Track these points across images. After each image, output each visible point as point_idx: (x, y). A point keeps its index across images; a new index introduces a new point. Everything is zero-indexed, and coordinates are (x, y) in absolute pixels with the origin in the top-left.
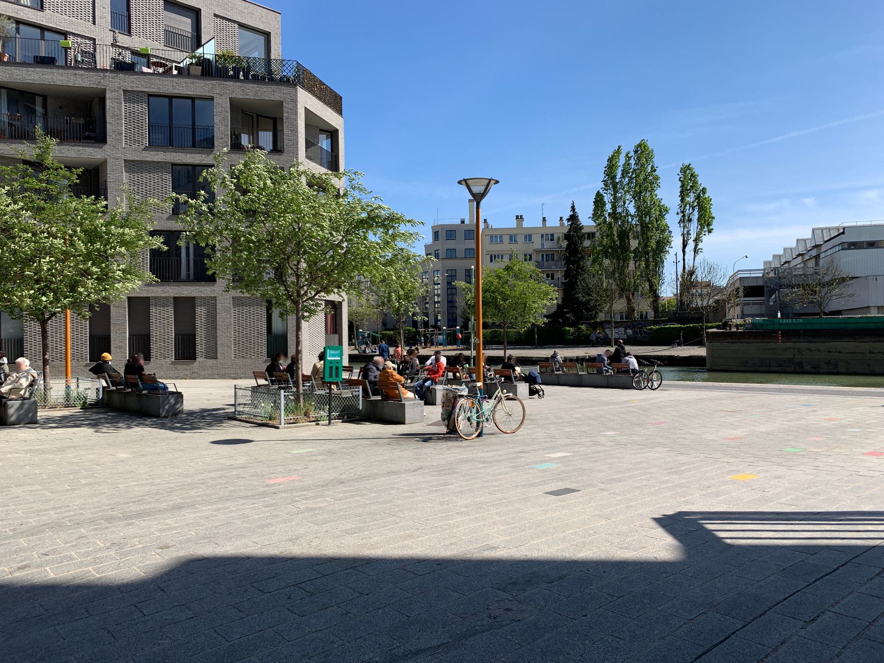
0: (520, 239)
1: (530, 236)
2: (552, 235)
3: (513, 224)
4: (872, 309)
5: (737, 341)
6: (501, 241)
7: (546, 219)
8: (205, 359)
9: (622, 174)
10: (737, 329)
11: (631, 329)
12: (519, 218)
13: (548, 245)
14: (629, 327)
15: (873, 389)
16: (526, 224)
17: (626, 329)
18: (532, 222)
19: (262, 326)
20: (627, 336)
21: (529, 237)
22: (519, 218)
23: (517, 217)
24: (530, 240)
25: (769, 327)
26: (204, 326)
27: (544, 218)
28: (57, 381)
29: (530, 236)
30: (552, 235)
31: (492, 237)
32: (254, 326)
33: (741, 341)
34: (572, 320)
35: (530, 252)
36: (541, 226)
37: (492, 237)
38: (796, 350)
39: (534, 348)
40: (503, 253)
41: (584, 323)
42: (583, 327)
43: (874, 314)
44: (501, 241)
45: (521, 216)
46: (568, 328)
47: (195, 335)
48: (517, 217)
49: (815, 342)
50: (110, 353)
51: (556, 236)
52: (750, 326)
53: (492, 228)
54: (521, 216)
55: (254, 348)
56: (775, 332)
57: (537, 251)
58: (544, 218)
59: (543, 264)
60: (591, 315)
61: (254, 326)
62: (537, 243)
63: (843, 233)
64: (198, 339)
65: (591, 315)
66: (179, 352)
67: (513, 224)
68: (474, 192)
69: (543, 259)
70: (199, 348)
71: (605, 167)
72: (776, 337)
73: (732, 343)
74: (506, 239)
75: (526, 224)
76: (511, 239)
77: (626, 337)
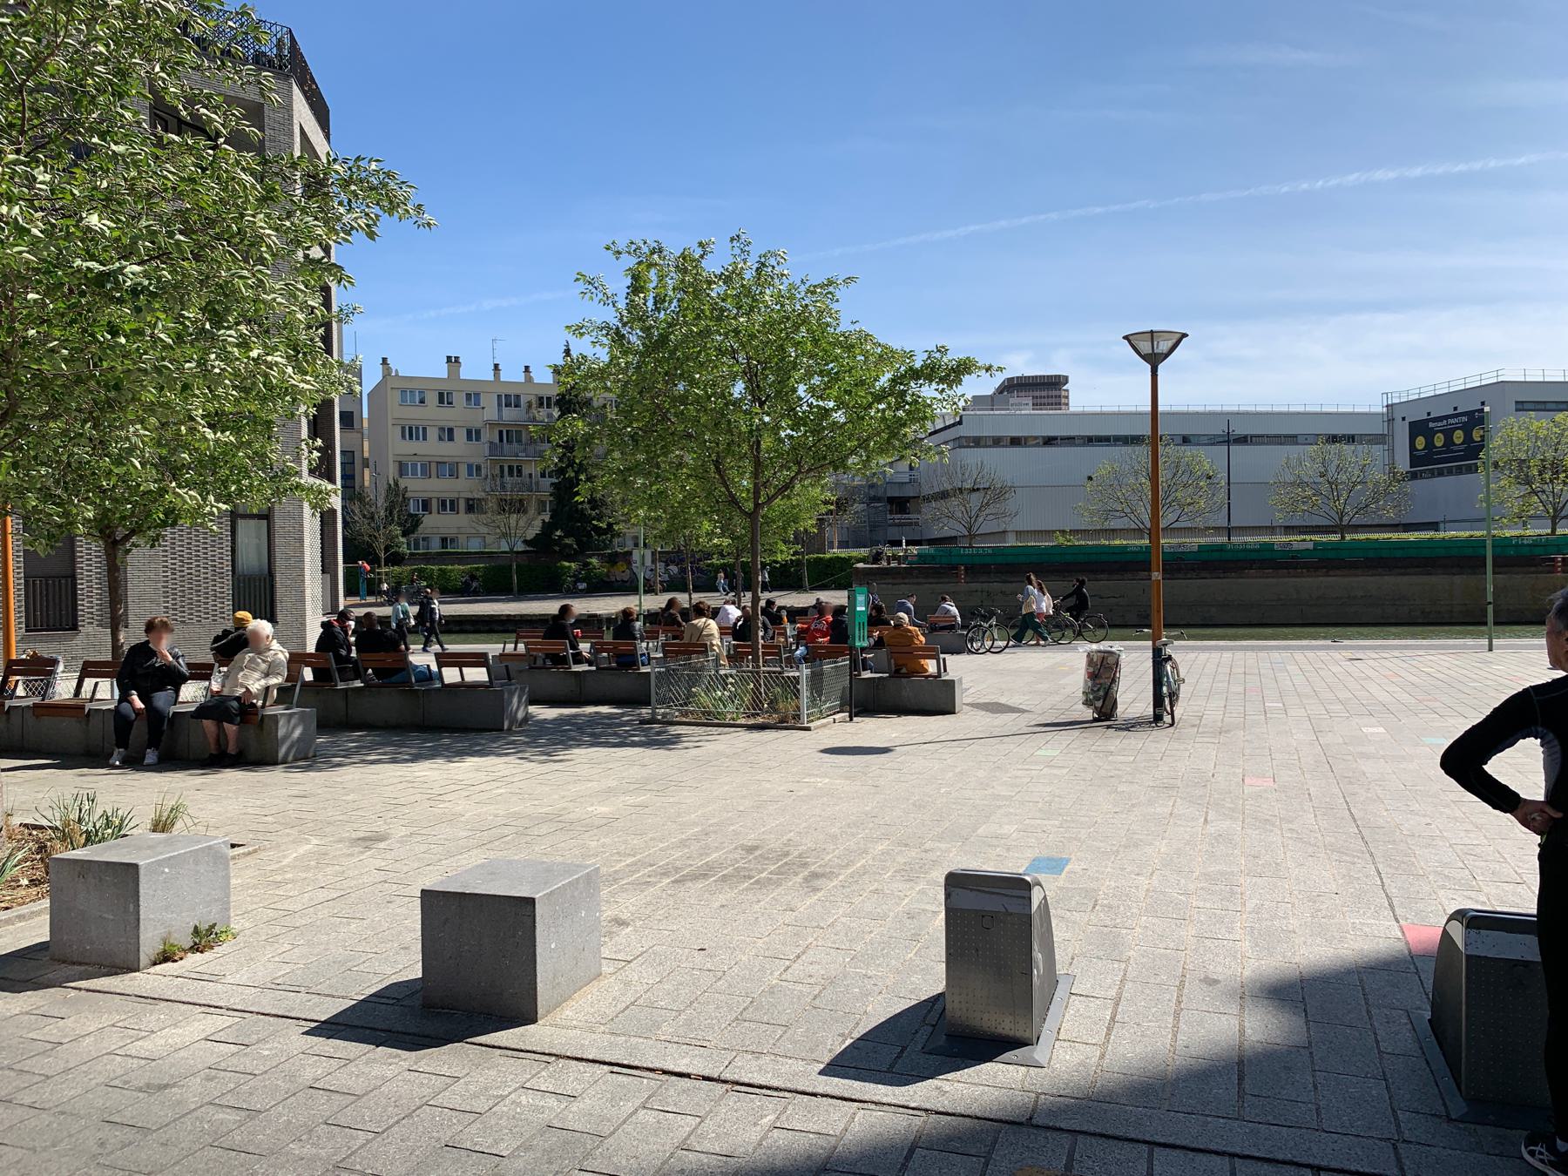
0: (459, 399)
1: (477, 395)
2: (518, 397)
3: (441, 371)
4: (1010, 534)
5: (902, 581)
6: (422, 401)
7: (500, 367)
8: (100, 629)
9: (655, 304)
10: (889, 564)
11: (677, 565)
12: (453, 361)
13: (509, 414)
14: (673, 562)
15: (1199, 643)
16: (466, 373)
17: (668, 565)
18: (475, 370)
19: (222, 558)
20: (670, 576)
21: (473, 397)
22: (453, 361)
23: (449, 358)
24: (477, 403)
25: (944, 560)
26: (96, 557)
27: (496, 366)
28: (1470, 642)
29: (477, 395)
30: (518, 397)
31: (404, 392)
32: (206, 558)
33: (906, 581)
34: (575, 549)
35: (478, 425)
36: (492, 379)
37: (404, 392)
38: (985, 594)
39: (513, 601)
40: (425, 423)
41: (594, 555)
42: (594, 561)
43: (1011, 542)
44: (422, 401)
45: (457, 358)
46: (567, 564)
47: (73, 577)
48: (449, 358)
49: (1011, 582)
50: (272, 619)
51: (523, 401)
52: (915, 559)
53: (397, 375)
54: (457, 358)
55: (207, 603)
56: (955, 567)
57: (492, 425)
58: (496, 366)
59: (502, 448)
60: (603, 541)
61: (206, 558)
62: (490, 411)
63: (960, 423)
64: (82, 585)
65: (603, 541)
66: (48, 615)
67: (441, 371)
68: (1149, 367)
69: (501, 440)
70: (84, 605)
71: (628, 287)
72: (957, 576)
73: (894, 584)
74: (432, 398)
75: (466, 373)
76: (441, 401)
77: (667, 579)
